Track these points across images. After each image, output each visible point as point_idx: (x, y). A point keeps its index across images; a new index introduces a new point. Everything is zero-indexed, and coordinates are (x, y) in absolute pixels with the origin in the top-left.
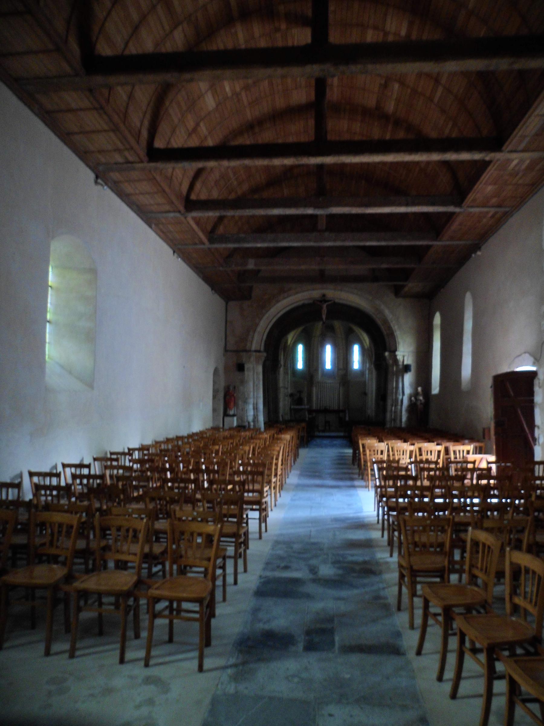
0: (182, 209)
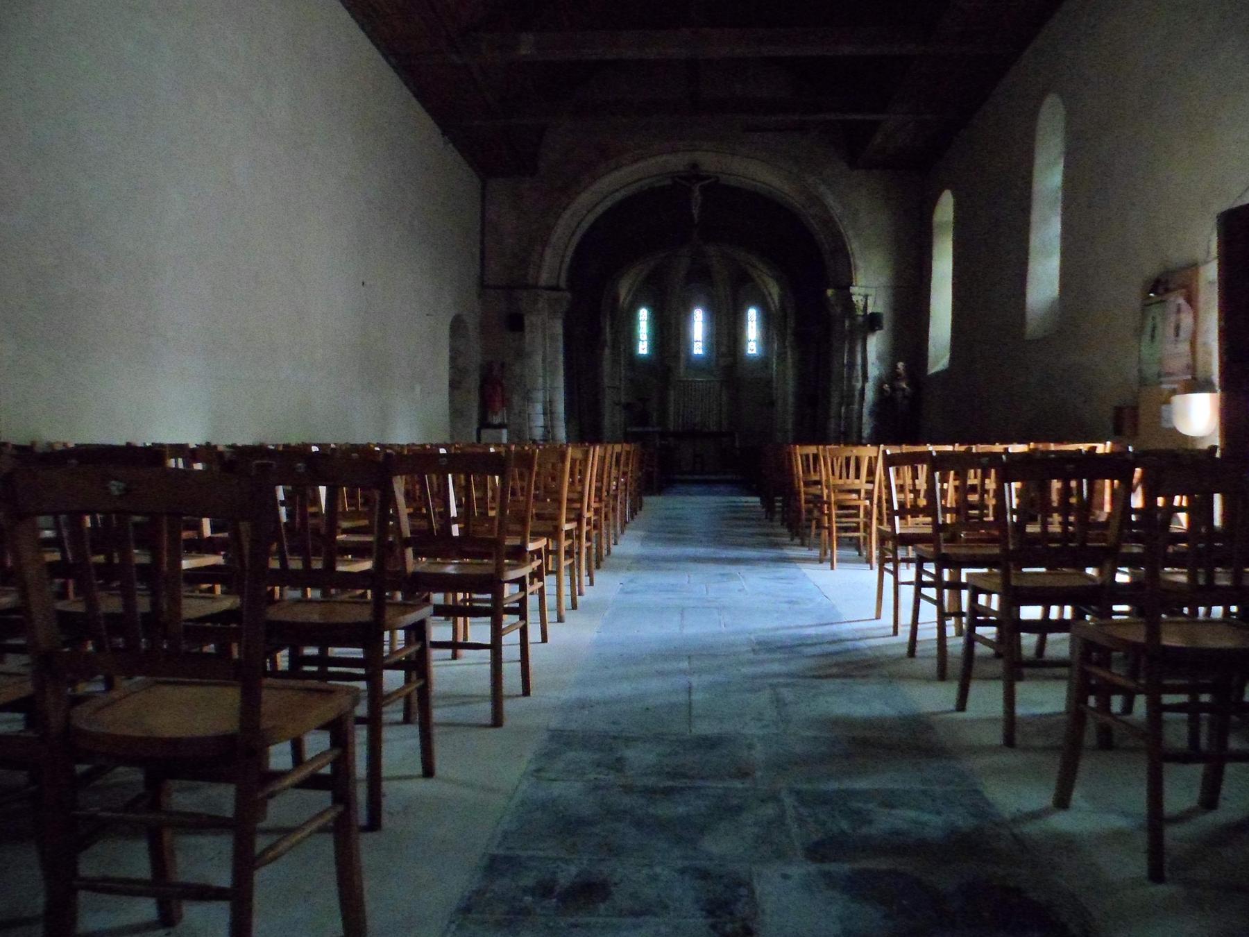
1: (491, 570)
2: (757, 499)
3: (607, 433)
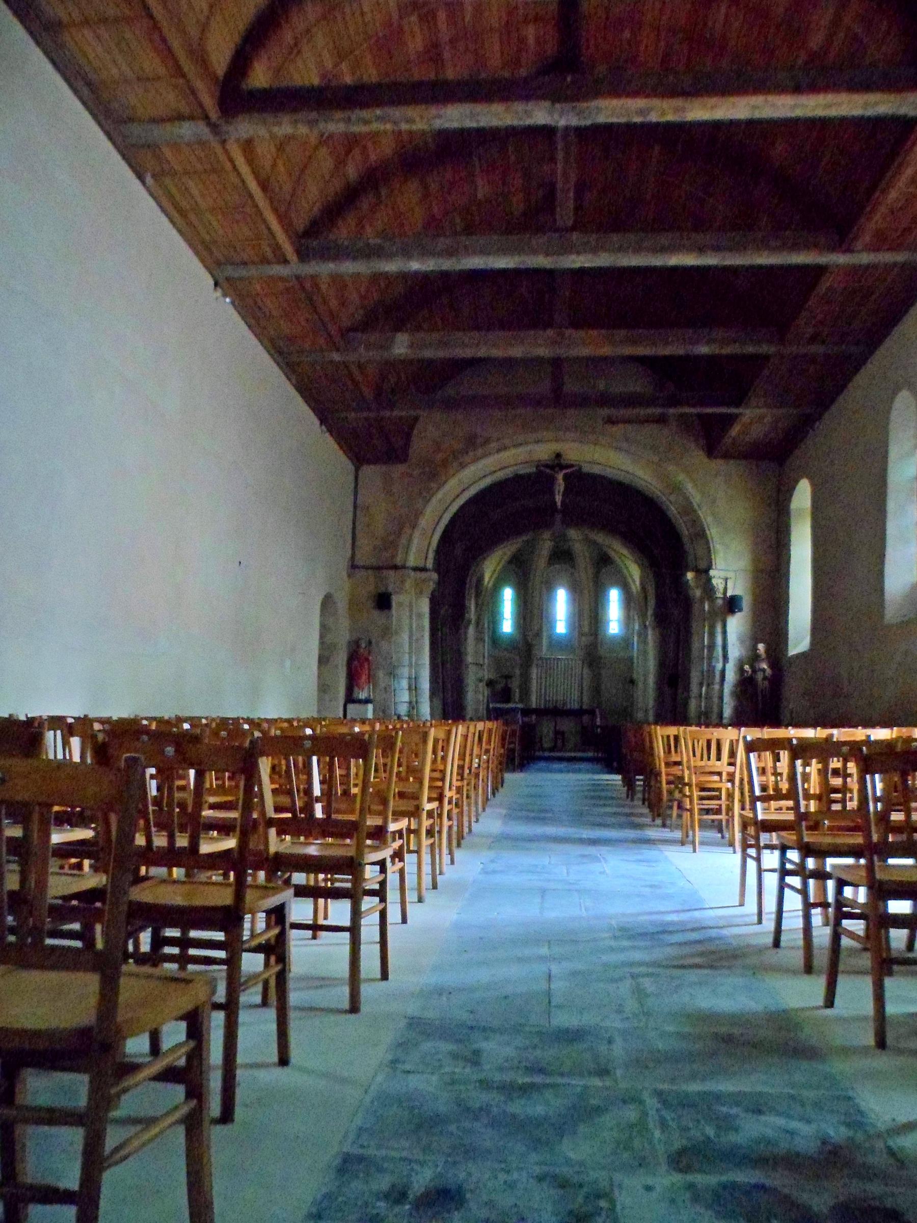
0: (214, 115)
1: (351, 852)
2: (619, 777)
3: (470, 711)
